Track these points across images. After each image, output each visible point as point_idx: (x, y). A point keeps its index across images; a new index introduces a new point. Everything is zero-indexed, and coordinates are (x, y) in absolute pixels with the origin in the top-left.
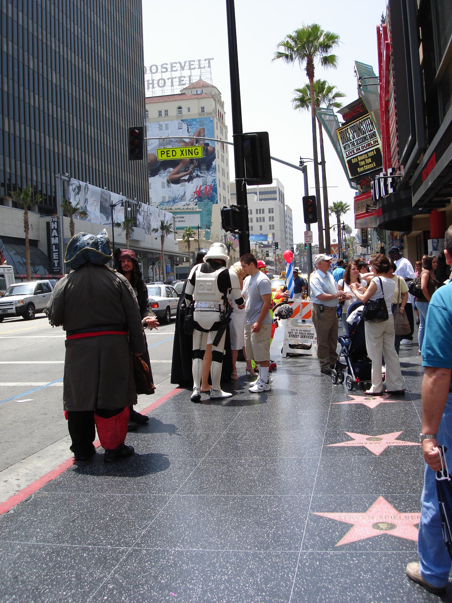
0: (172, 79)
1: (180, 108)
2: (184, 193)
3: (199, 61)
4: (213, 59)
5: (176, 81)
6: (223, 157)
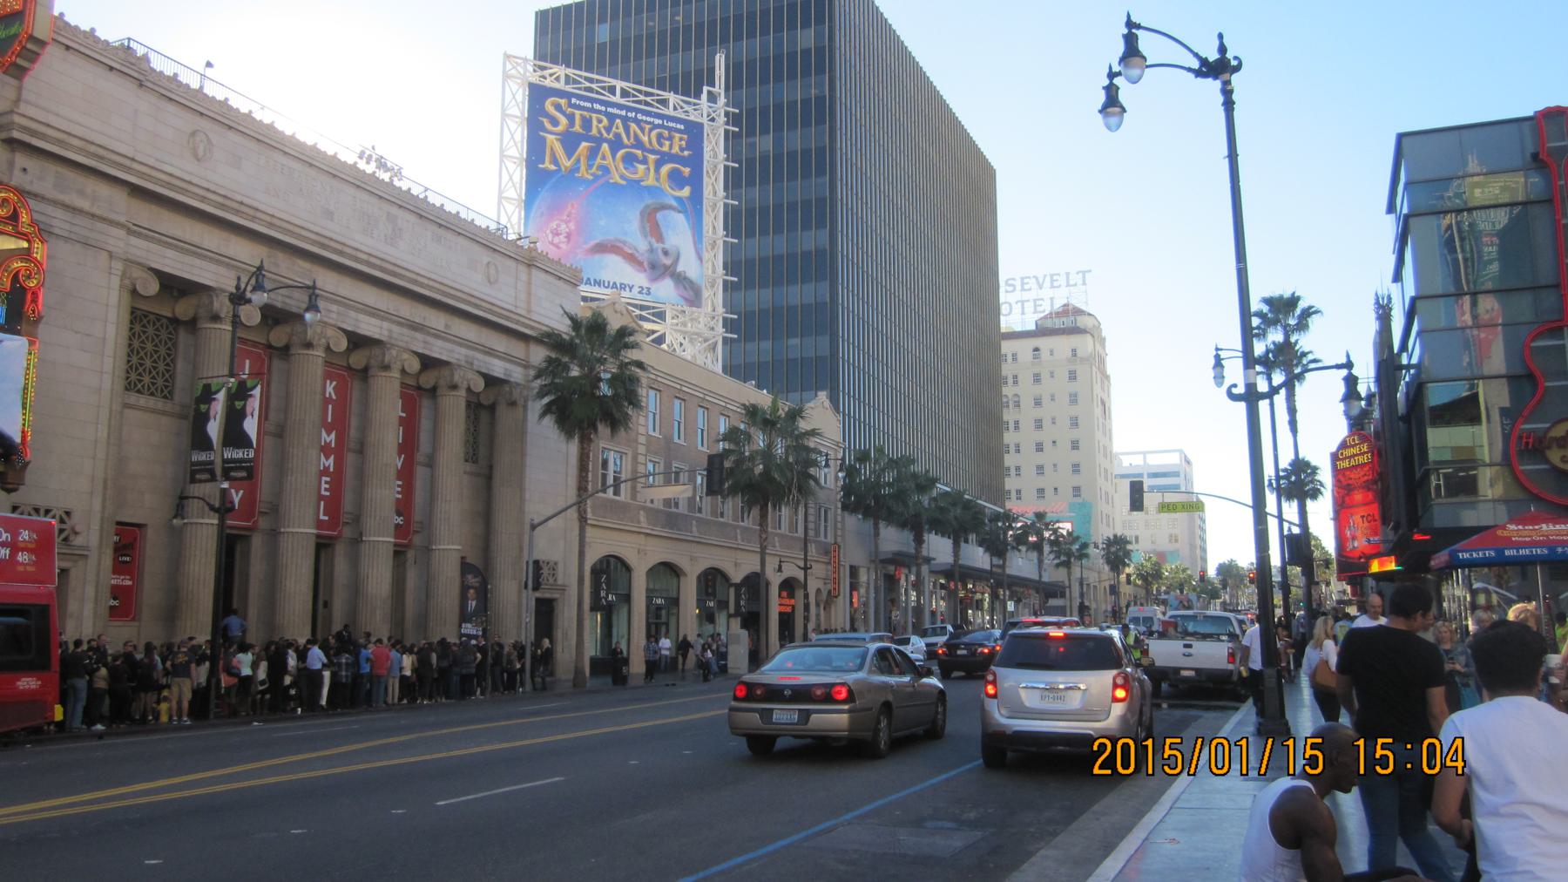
0: (1023, 302)
1: (1036, 350)
2: (1217, 43)
3: (1068, 274)
4: (1221, 36)
5: (1029, 307)
6: (1104, 426)
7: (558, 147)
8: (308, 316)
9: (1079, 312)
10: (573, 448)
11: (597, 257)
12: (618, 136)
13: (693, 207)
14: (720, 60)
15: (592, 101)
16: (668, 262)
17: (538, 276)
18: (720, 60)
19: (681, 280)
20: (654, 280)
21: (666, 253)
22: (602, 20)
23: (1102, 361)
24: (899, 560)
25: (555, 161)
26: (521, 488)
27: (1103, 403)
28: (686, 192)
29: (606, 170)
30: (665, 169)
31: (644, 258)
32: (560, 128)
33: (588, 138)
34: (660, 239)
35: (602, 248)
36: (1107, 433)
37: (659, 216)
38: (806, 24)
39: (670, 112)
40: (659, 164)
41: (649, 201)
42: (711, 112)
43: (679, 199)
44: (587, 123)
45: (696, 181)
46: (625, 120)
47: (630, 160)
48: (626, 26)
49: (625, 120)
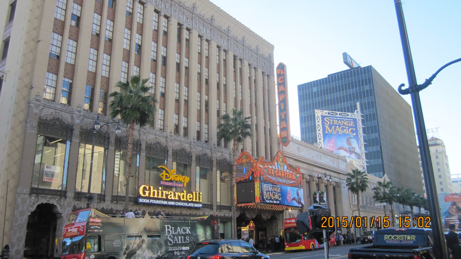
7: (328, 128)
8: (330, 180)
9: (437, 139)
10: (356, 196)
11: (339, 151)
12: (340, 124)
13: (357, 137)
14: (358, 104)
15: (334, 117)
16: (353, 150)
17: (340, 160)
18: (358, 104)
19: (356, 153)
20: (350, 154)
21: (352, 148)
22: (314, 86)
23: (445, 152)
24: (407, 213)
25: (328, 131)
26: (342, 203)
27: (447, 164)
28: (355, 134)
29: (338, 131)
30: (350, 130)
31: (348, 150)
32: (328, 124)
33: (334, 125)
34: (351, 145)
35: (339, 148)
36: (449, 172)
37: (350, 140)
38: (366, 84)
39: (349, 117)
40: (348, 129)
41: (347, 137)
42: (357, 115)
43: (353, 136)
44: (333, 122)
45: (356, 131)
46: (341, 120)
47: (343, 129)
48: (321, 88)
49: (341, 120)
